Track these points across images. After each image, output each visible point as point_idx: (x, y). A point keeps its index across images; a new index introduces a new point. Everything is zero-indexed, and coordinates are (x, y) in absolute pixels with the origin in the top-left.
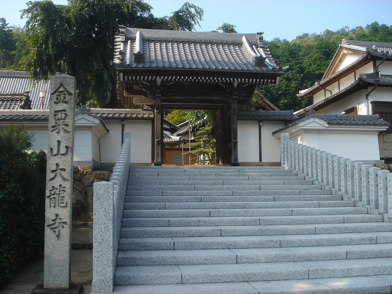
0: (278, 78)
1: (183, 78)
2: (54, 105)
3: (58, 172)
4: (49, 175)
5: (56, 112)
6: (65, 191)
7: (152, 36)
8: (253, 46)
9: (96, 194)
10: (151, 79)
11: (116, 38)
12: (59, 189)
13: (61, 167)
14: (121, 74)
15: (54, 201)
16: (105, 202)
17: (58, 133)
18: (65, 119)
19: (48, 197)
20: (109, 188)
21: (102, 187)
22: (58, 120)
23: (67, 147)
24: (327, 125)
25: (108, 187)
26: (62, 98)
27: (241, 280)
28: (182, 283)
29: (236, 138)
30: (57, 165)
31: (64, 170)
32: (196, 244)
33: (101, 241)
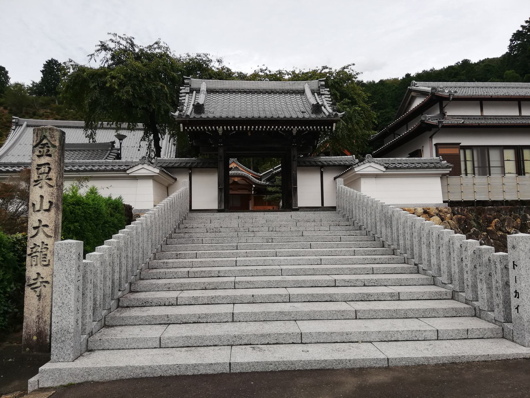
0: (334, 124)
1: (281, 127)
2: (37, 158)
3: (40, 228)
4: (31, 232)
5: (38, 165)
6: (48, 248)
7: (217, 87)
8: (316, 94)
9: (57, 254)
10: (266, 129)
11: (181, 89)
12: (41, 246)
13: (43, 223)
14: (181, 125)
15: (35, 260)
16: (67, 263)
17: (41, 187)
18: (48, 173)
19: (29, 255)
20: (71, 247)
21: (64, 246)
22: (41, 174)
23: (50, 202)
24: (384, 170)
25: (70, 246)
26: (45, 151)
27: (225, 343)
28: (160, 347)
29: (296, 184)
30: (40, 221)
31: (46, 226)
32: (200, 298)
33: (61, 305)
